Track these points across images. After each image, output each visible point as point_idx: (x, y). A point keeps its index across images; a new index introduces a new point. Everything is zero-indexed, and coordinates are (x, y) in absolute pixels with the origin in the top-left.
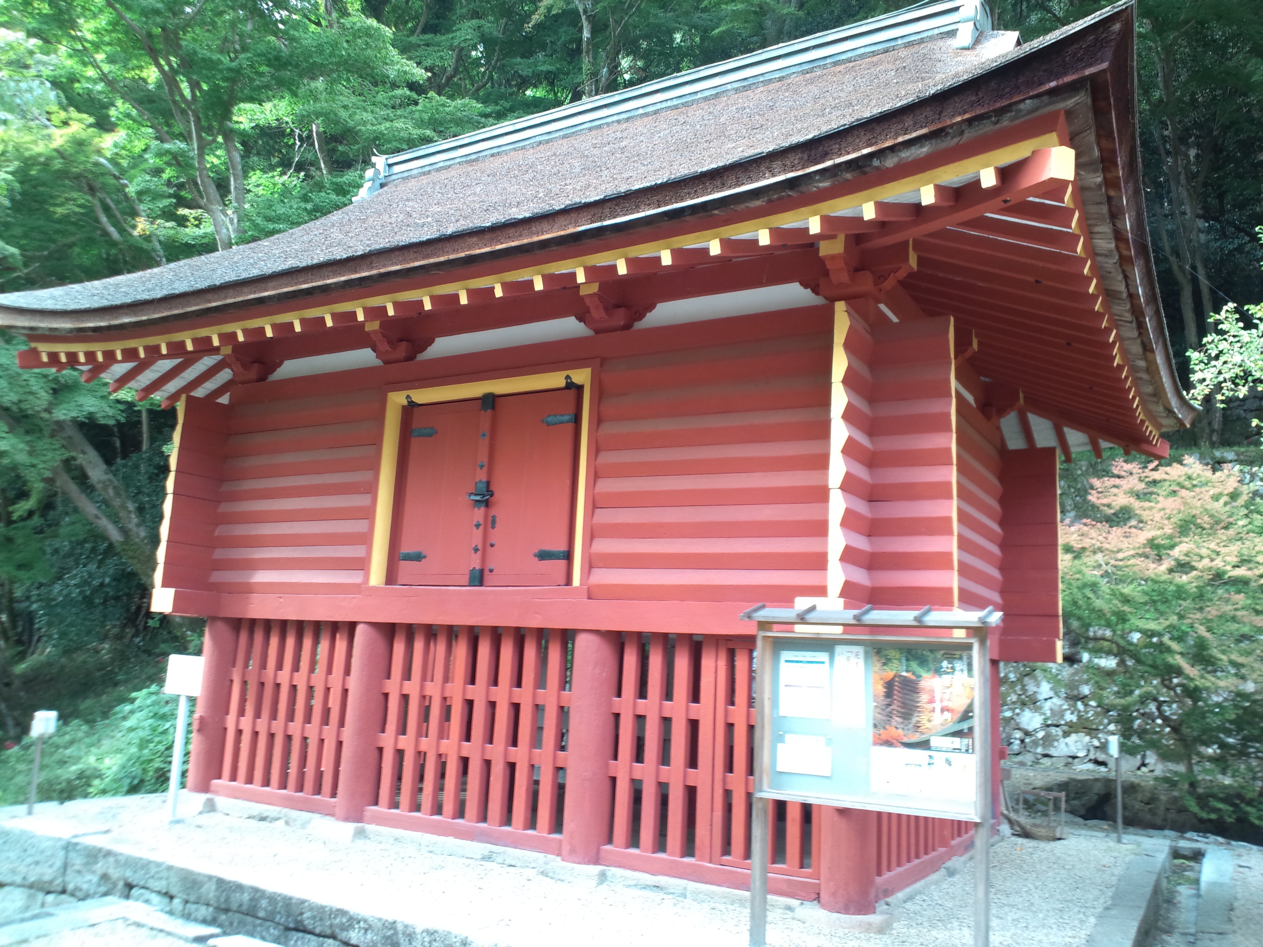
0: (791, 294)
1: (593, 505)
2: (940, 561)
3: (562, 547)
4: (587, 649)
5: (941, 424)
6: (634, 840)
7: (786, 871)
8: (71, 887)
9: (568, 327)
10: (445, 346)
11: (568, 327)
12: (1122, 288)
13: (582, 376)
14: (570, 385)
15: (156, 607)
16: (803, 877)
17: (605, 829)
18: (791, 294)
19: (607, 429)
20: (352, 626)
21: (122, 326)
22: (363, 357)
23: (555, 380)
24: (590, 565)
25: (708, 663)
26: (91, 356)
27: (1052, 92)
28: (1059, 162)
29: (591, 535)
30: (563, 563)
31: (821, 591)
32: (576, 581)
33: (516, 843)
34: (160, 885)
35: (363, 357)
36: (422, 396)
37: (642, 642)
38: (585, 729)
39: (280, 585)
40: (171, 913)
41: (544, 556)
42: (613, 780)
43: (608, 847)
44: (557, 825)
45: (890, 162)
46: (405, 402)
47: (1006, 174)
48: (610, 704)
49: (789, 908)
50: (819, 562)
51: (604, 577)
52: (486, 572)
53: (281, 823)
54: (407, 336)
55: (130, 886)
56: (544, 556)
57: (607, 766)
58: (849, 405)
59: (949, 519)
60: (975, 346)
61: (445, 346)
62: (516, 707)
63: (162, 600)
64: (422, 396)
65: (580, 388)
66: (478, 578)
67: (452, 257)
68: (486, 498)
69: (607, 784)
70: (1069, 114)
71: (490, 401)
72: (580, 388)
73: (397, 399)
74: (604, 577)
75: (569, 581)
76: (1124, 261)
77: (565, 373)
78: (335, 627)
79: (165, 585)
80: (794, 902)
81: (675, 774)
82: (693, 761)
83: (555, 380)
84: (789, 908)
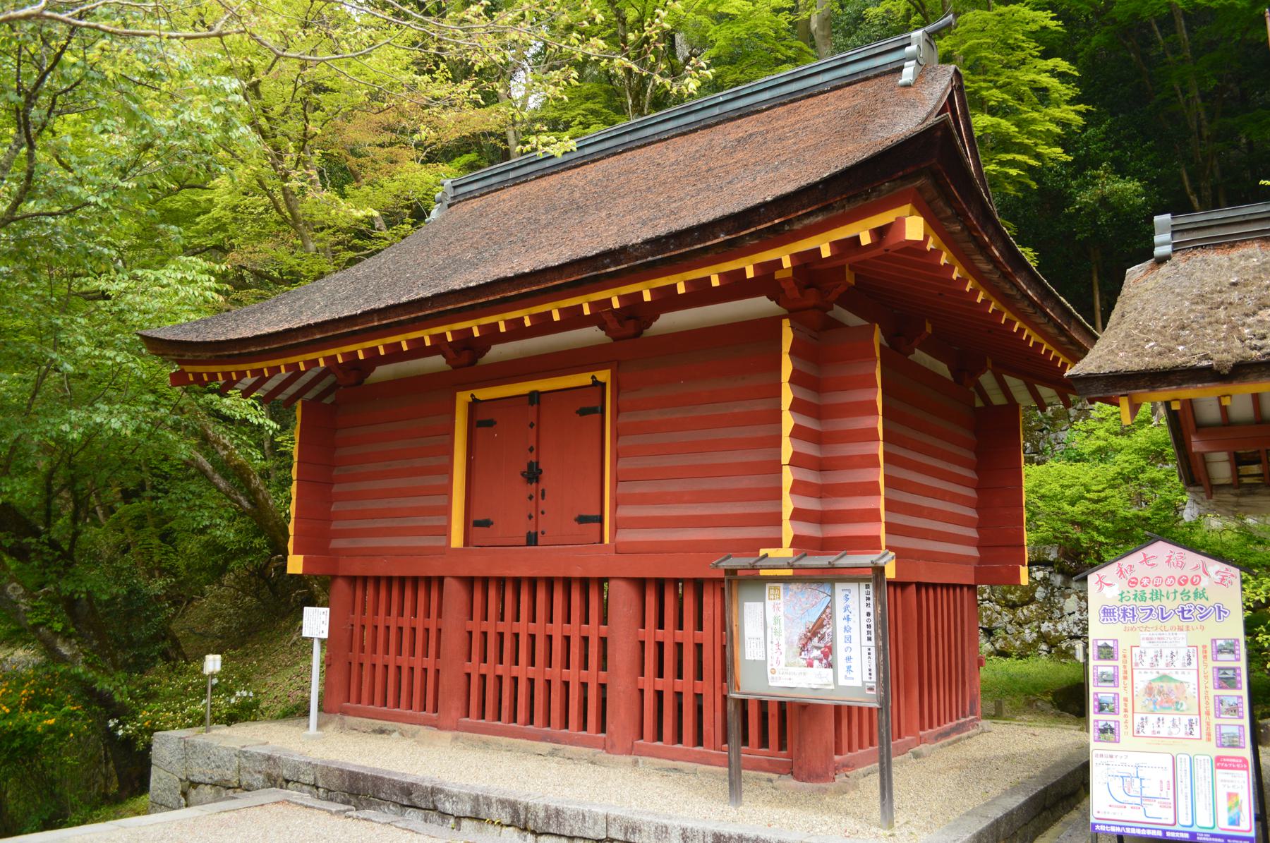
0: (761, 305)
1: (616, 480)
2: (872, 515)
3: (598, 513)
4: (452, 587)
5: (870, 409)
6: (659, 736)
7: (770, 754)
8: (244, 783)
9: (592, 334)
10: (498, 351)
11: (592, 334)
12: (1014, 292)
13: (604, 376)
14: (596, 383)
15: (290, 571)
16: (782, 757)
17: (637, 729)
18: (761, 305)
19: (623, 418)
20: (441, 579)
21: (251, 354)
22: (437, 362)
23: (584, 379)
24: (616, 528)
25: (707, 600)
26: (227, 375)
27: (901, 178)
28: (914, 228)
29: (616, 504)
30: (598, 525)
31: (777, 543)
32: (607, 541)
33: (572, 742)
34: (309, 779)
35: (437, 362)
36: (483, 394)
37: (660, 585)
38: (622, 654)
39: (383, 544)
40: (319, 798)
41: (582, 520)
42: (642, 691)
43: (641, 741)
44: (602, 728)
45: (797, 226)
46: (470, 400)
47: (879, 233)
48: (637, 634)
49: (770, 780)
50: (776, 520)
51: (626, 536)
52: (540, 534)
53: (395, 735)
54: (467, 352)
55: (287, 781)
56: (582, 520)
57: (637, 681)
58: (794, 399)
59: (877, 483)
60: (929, 329)
61: (498, 351)
62: (567, 639)
63: (295, 564)
64: (483, 394)
65: (604, 384)
66: (532, 540)
67: (491, 298)
68: (533, 474)
69: (636, 695)
70: (919, 189)
71: (534, 397)
72: (604, 384)
73: (463, 398)
74: (626, 536)
75: (602, 541)
76: (1005, 276)
77: (592, 374)
78: (428, 580)
79: (295, 553)
80: (774, 776)
81: (687, 685)
82: (699, 675)
83: (584, 379)
84: (770, 780)
